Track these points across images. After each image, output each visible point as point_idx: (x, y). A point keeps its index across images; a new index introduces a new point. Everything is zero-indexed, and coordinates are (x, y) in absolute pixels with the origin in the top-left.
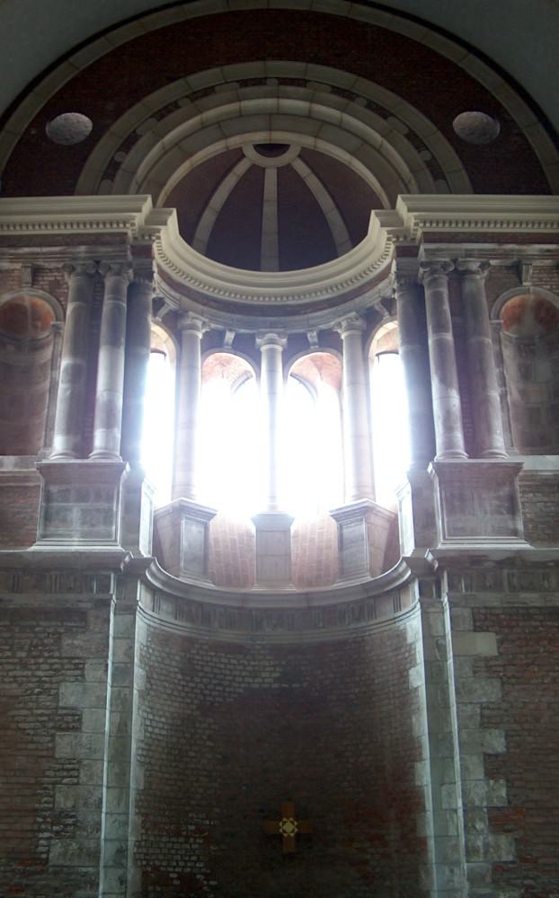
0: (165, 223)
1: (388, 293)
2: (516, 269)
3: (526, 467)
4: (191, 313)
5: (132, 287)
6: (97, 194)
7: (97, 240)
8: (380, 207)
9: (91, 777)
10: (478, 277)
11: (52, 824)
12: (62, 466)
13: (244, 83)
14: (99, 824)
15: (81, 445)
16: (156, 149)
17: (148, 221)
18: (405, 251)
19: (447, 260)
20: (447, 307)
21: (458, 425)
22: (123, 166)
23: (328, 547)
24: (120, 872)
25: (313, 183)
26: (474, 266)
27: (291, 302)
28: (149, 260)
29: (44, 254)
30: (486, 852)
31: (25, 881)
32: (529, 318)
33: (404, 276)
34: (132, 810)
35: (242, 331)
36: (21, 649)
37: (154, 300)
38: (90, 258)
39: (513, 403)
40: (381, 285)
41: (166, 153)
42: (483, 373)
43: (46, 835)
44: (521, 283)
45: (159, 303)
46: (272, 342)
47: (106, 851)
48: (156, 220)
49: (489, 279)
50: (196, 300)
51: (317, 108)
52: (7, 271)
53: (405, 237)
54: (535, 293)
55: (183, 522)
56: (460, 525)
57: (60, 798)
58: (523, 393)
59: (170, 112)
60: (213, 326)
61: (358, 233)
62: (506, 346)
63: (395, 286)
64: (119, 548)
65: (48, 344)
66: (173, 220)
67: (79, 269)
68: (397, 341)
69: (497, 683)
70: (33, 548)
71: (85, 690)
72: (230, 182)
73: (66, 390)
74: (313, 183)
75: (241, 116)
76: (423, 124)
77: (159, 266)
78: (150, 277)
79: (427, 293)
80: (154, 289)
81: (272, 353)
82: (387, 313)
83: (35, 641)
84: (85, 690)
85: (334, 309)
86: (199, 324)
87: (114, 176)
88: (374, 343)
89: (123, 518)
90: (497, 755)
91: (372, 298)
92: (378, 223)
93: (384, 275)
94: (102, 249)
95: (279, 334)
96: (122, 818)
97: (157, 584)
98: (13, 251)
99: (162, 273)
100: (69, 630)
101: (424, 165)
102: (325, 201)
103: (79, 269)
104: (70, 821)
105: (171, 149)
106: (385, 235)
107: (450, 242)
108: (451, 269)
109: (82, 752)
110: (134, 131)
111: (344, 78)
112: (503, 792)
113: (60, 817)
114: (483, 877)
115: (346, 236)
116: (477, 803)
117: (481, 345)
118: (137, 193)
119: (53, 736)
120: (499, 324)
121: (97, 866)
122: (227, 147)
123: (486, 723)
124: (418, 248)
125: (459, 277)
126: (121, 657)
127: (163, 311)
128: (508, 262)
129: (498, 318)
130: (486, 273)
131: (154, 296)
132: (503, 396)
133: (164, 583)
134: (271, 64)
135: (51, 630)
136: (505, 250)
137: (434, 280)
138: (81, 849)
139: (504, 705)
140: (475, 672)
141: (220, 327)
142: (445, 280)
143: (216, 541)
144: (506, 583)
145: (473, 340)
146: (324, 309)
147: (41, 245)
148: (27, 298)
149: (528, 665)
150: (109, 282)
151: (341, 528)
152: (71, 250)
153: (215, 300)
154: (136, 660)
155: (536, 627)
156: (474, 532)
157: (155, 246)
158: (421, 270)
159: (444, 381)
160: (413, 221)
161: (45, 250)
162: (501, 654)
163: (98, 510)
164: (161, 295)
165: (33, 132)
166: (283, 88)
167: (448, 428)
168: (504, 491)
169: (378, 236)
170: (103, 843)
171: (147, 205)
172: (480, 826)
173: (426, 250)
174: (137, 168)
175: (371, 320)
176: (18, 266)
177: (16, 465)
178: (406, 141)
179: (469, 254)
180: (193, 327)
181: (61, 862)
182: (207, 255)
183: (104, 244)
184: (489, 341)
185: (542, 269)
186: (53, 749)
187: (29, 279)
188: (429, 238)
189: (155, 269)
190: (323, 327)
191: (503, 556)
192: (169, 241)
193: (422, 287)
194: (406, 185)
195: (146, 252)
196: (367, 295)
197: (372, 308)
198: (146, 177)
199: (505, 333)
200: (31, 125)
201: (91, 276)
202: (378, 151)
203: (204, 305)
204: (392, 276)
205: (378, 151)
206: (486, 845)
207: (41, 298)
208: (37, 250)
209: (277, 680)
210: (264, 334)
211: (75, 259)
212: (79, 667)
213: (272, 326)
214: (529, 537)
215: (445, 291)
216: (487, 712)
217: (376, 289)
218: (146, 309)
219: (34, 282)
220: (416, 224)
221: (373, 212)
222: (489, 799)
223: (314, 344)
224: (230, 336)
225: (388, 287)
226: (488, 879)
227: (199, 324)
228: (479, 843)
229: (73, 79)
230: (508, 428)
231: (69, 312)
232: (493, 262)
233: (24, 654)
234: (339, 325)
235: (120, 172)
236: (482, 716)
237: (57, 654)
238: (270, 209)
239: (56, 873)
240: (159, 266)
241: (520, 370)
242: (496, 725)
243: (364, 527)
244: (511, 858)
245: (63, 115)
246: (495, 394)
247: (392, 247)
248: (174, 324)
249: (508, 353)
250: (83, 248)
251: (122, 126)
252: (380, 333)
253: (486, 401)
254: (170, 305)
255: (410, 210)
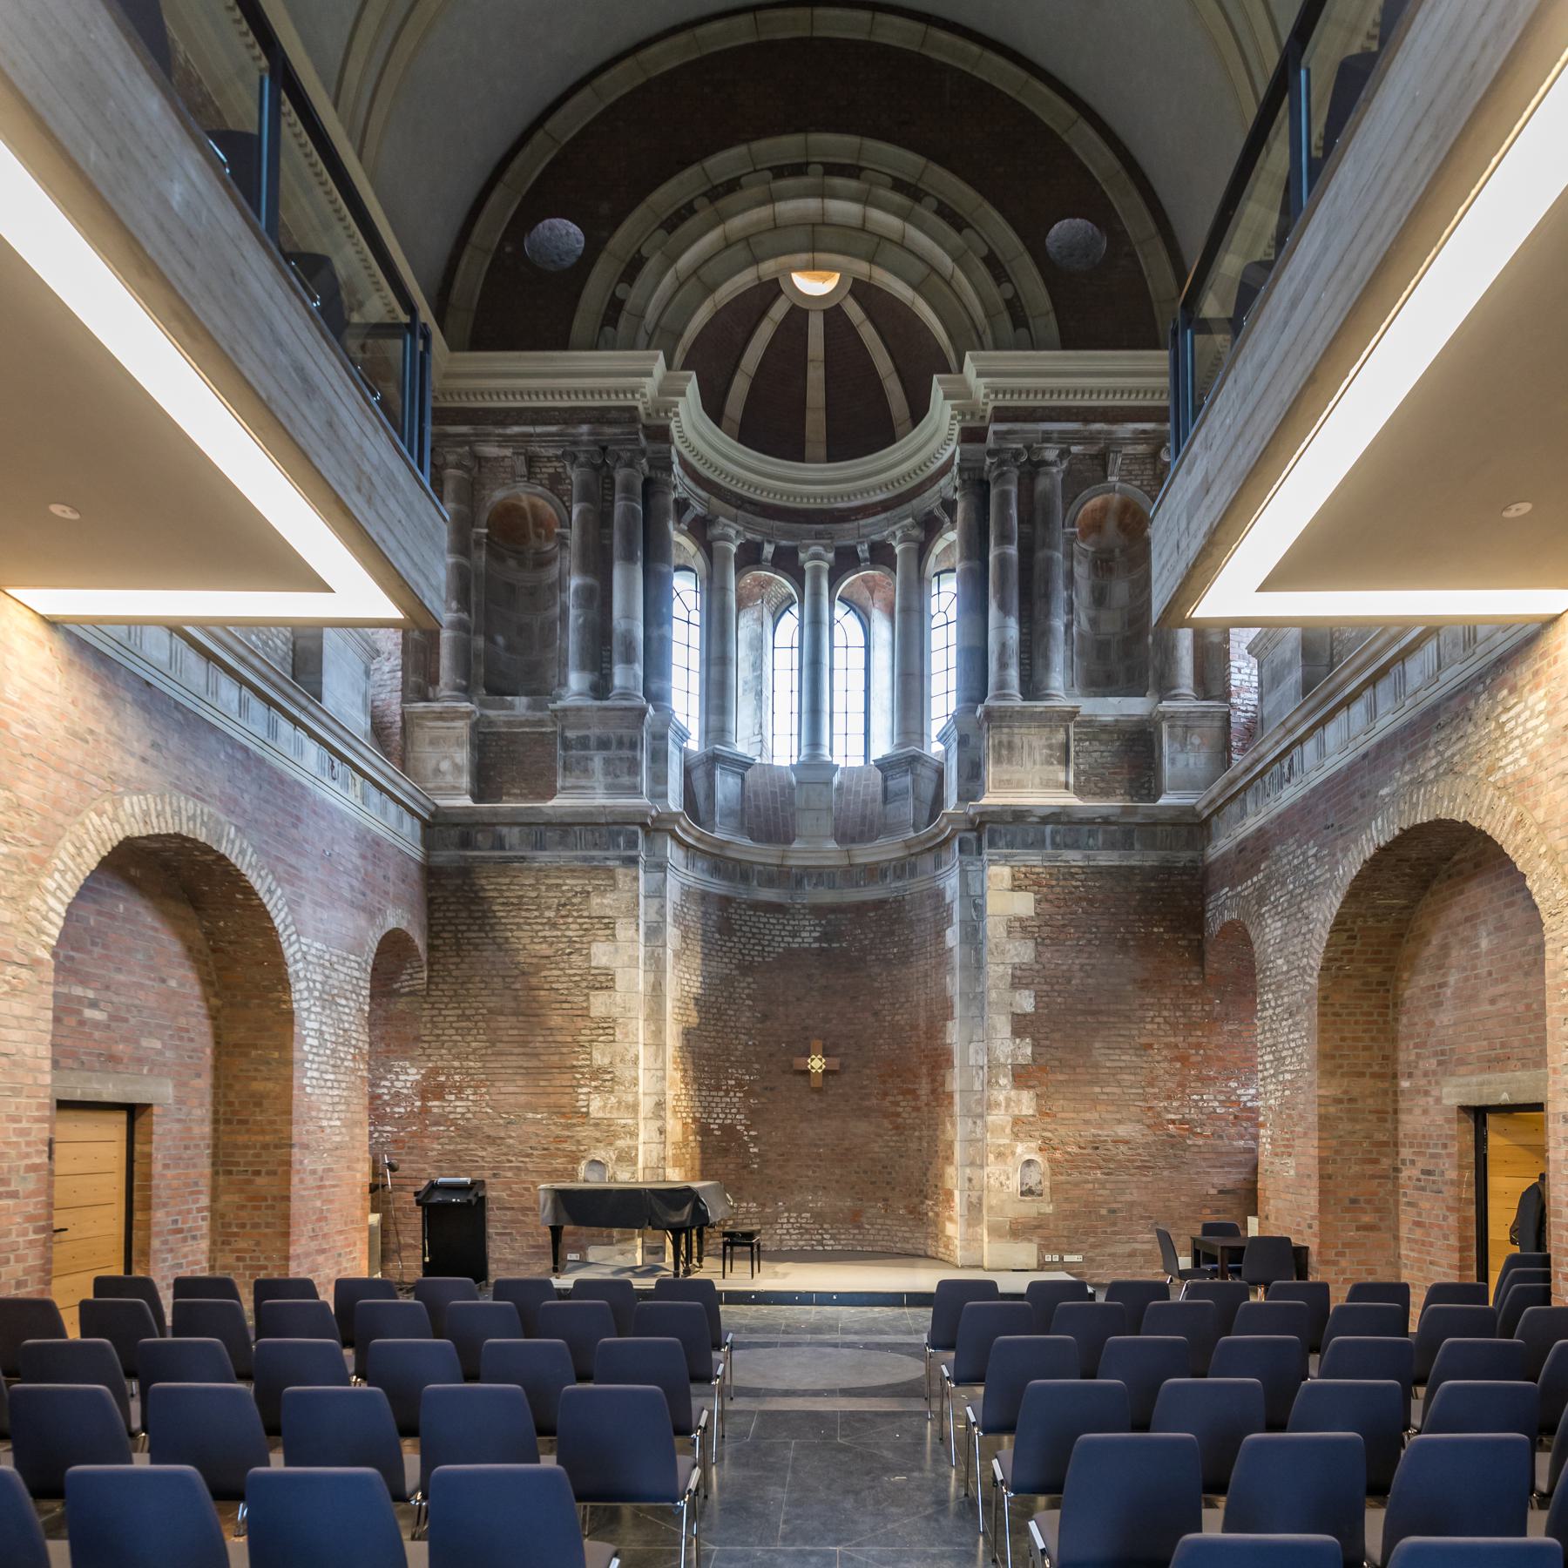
0: (682, 394)
1: (949, 493)
2: (1101, 461)
3: (1083, 711)
4: (721, 519)
5: (648, 482)
6: (596, 348)
7: (599, 416)
8: (946, 370)
9: (626, 1035)
10: (1054, 470)
11: (592, 1079)
12: (579, 709)
13: (779, 172)
14: (636, 1079)
15: (601, 688)
16: (668, 280)
17: (662, 391)
18: (971, 435)
19: (1020, 446)
20: (1014, 512)
21: (1014, 661)
22: (628, 306)
23: (874, 800)
24: (659, 1123)
25: (868, 333)
26: (1051, 454)
27: (840, 505)
28: (664, 446)
29: (539, 435)
30: (1007, 1106)
31: (567, 1133)
32: (1111, 526)
33: (969, 469)
34: (670, 1066)
35: (784, 543)
36: (549, 908)
37: (676, 501)
38: (595, 442)
39: (1081, 635)
40: (943, 482)
41: (681, 285)
42: (1047, 597)
43: (585, 1090)
44: (1106, 477)
45: (682, 506)
46: (817, 557)
47: (646, 1105)
48: (670, 390)
49: (1068, 473)
50: (727, 502)
51: (876, 215)
52: (496, 459)
53: (973, 414)
54: (1121, 491)
55: (718, 772)
56: (1006, 777)
57: (596, 1055)
58: (1094, 622)
59: (683, 219)
60: (749, 536)
61: (919, 410)
62: (1079, 563)
63: (957, 482)
64: (645, 801)
65: (555, 559)
66: (692, 387)
67: (582, 458)
68: (955, 559)
69: (1031, 944)
70: (550, 803)
71: (616, 950)
72: (765, 331)
73: (578, 617)
74: (868, 333)
75: (776, 227)
76: (1007, 239)
77: (679, 454)
78: (669, 469)
79: (994, 492)
80: (675, 487)
81: (817, 572)
82: (947, 519)
83: (563, 901)
84: (616, 950)
85: (888, 514)
86: (732, 533)
87: (617, 321)
88: (932, 560)
89: (649, 768)
90: (1025, 1015)
91: (929, 501)
92: (941, 393)
93: (944, 470)
94: (609, 431)
95: (824, 546)
96: (660, 1073)
97: (690, 840)
98: (500, 431)
99: (685, 464)
100: (596, 888)
101: (1002, 306)
102: (883, 362)
103: (582, 458)
104: (608, 1077)
105: (688, 278)
106: (948, 412)
107: (1025, 421)
108: (1023, 459)
109: (616, 1012)
110: (639, 251)
111: (908, 162)
112: (1029, 1051)
113: (597, 1073)
114: (1003, 1130)
115: (906, 412)
116: (1002, 1060)
117: (1049, 561)
118: (648, 348)
119: (587, 995)
120: (1073, 533)
121: (635, 1118)
122: (759, 278)
123: (1017, 983)
124: (986, 429)
125: (1034, 468)
126: (654, 917)
127: (689, 516)
128: (1094, 450)
129: (1073, 526)
130: (1065, 464)
131: (674, 495)
132: (1068, 626)
133: (698, 839)
134: (817, 138)
135: (578, 889)
136: (1091, 432)
137: (1002, 475)
138: (619, 1103)
139: (1037, 967)
140: (1009, 932)
141: (758, 538)
142: (1014, 474)
143: (756, 794)
144: (1048, 841)
145: (1040, 555)
146: (874, 514)
147: (534, 423)
148: (524, 497)
149: (1064, 926)
150: (620, 475)
151: (885, 780)
152: (571, 430)
153: (752, 502)
154: (669, 919)
155: (1076, 887)
156: (1020, 785)
157: (673, 425)
158: (988, 461)
159: (1004, 608)
160: (983, 391)
161: (539, 429)
162: (1037, 914)
163: (621, 759)
164: (685, 495)
165: (508, 249)
166: (721, 203)
167: (1003, 666)
168: (1060, 737)
169: (942, 413)
170: (641, 1097)
171: (659, 367)
172: (1003, 1081)
173: (995, 433)
174: (646, 307)
175: (930, 527)
176: (508, 452)
177: (529, 707)
178: (982, 267)
179: (1047, 437)
180: (726, 538)
181: (601, 1115)
182: (740, 441)
183: (610, 423)
184: (1059, 555)
185: (1134, 458)
186: (587, 1008)
187: (524, 470)
188: (1001, 414)
189: (675, 459)
190: (875, 538)
191: (1048, 811)
192: (689, 419)
193: (988, 483)
194: (980, 337)
195: (661, 434)
196: (926, 495)
197: (931, 512)
198: (657, 325)
199: (1081, 545)
200: (503, 239)
201: (596, 468)
202: (948, 284)
203: (738, 507)
204: (955, 469)
205: (948, 284)
206: (1008, 1100)
207: (540, 496)
208: (530, 429)
209: (816, 940)
210: (808, 546)
211: (575, 443)
212: (610, 926)
213: (818, 536)
214: (1080, 791)
215: (1013, 489)
216: (1018, 973)
217: (936, 488)
218: (666, 513)
219: (530, 475)
220: (986, 396)
221: (935, 377)
222: (1014, 1056)
223: (866, 560)
224: (769, 550)
225: (948, 485)
226: (1008, 1130)
227: (732, 533)
228: (1001, 1098)
229: (551, 163)
230: (1070, 665)
231: (574, 517)
232: (1075, 449)
233: (552, 914)
234: (893, 534)
235: (624, 315)
236: (1013, 976)
237: (585, 914)
238: (816, 375)
239: (596, 1125)
240: (679, 454)
241: (1093, 592)
242: (1027, 986)
243: (909, 779)
244: (1031, 1112)
245: (547, 222)
246: (1059, 624)
247: (957, 428)
248: (701, 530)
249: (1081, 571)
250: (585, 428)
251: (621, 240)
252: (939, 546)
253: (1047, 632)
254: (698, 509)
255: (979, 375)
